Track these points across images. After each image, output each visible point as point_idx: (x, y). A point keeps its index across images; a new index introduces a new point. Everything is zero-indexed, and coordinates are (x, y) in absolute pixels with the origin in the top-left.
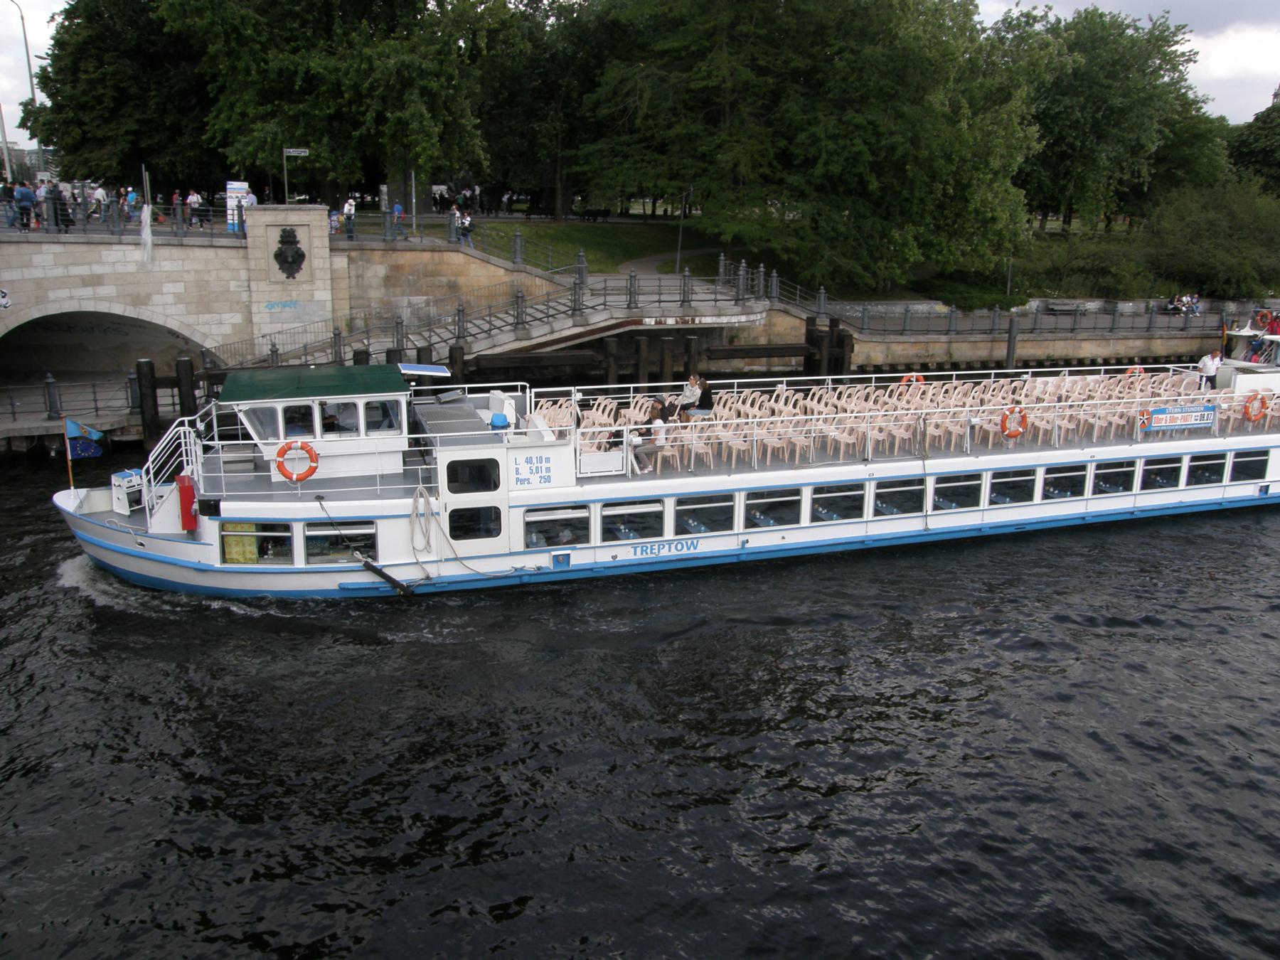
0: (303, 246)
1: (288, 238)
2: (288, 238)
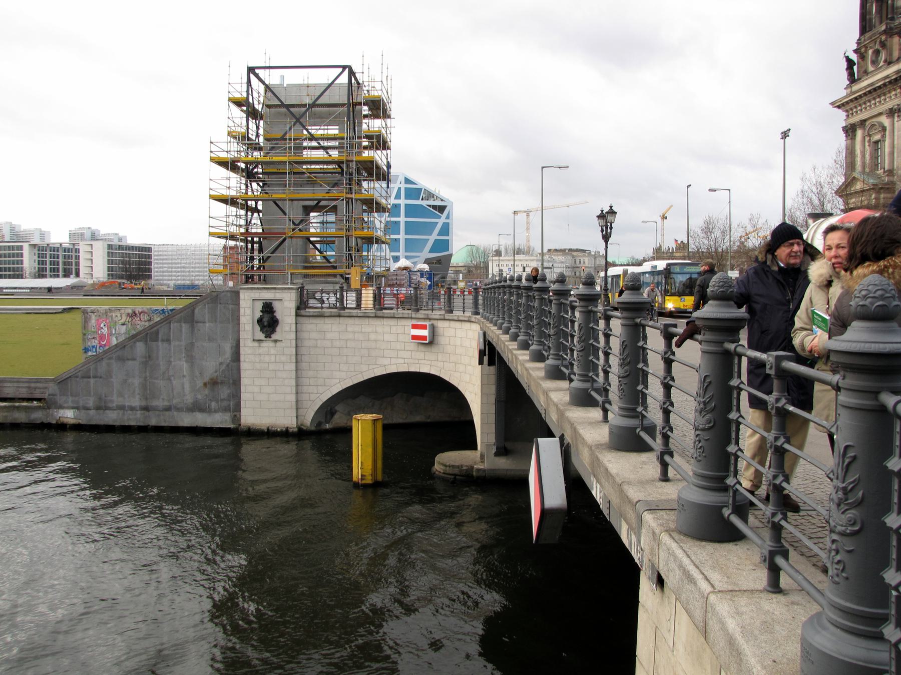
0: (278, 315)
1: (268, 308)
2: (268, 308)
